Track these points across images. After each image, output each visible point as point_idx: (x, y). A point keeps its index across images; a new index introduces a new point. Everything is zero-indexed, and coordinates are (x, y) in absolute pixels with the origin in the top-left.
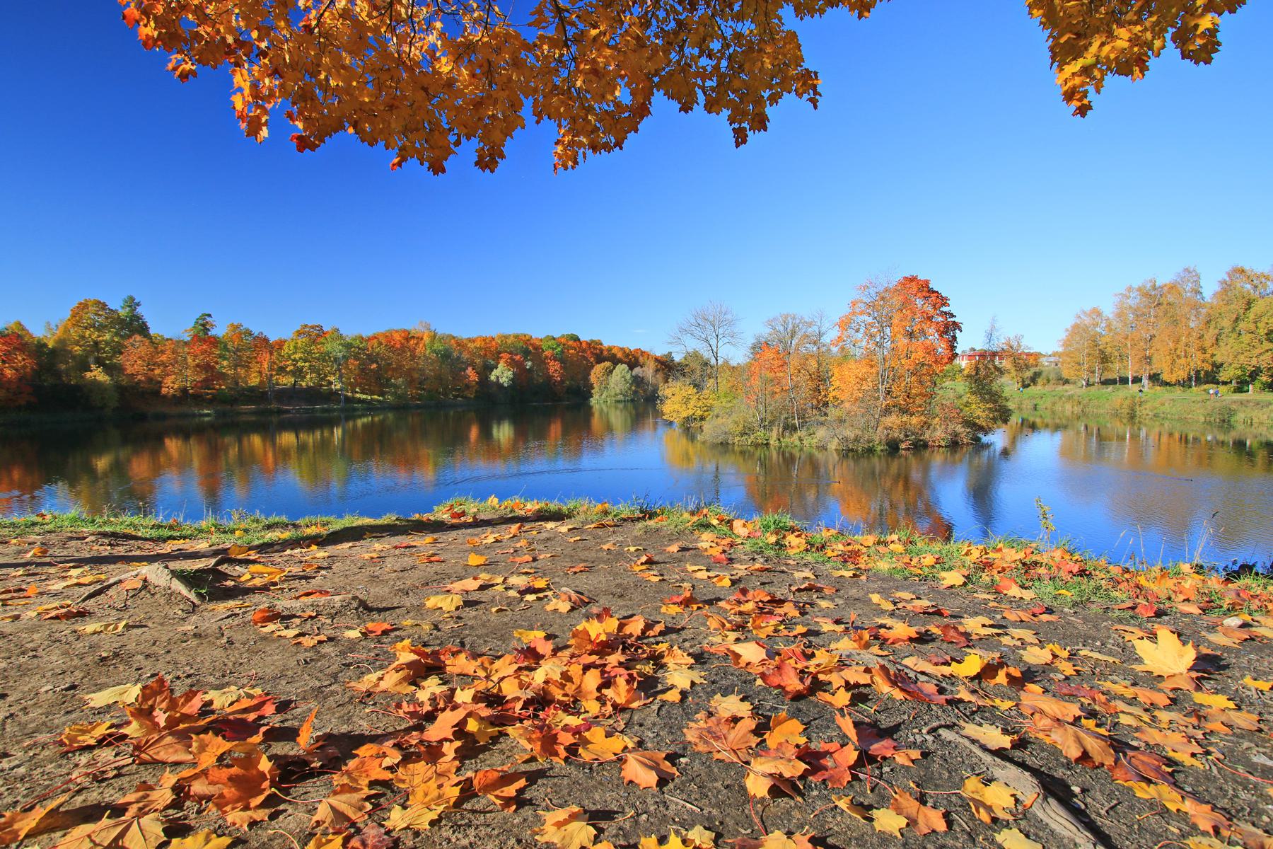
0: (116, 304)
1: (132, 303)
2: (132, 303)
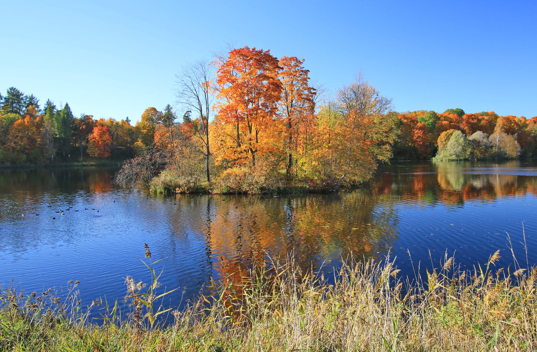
0: (161, 109)
1: (168, 108)
2: (168, 108)
